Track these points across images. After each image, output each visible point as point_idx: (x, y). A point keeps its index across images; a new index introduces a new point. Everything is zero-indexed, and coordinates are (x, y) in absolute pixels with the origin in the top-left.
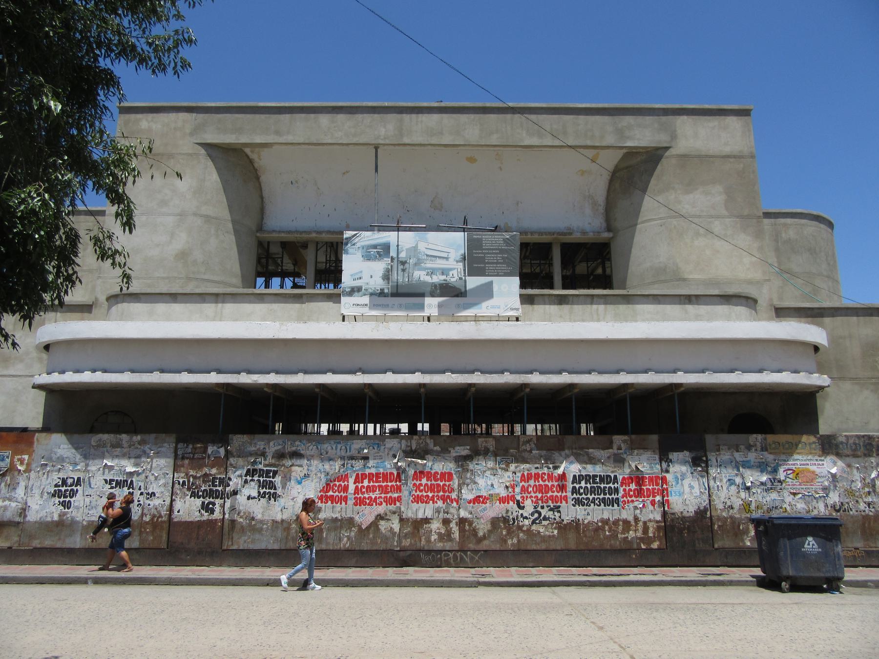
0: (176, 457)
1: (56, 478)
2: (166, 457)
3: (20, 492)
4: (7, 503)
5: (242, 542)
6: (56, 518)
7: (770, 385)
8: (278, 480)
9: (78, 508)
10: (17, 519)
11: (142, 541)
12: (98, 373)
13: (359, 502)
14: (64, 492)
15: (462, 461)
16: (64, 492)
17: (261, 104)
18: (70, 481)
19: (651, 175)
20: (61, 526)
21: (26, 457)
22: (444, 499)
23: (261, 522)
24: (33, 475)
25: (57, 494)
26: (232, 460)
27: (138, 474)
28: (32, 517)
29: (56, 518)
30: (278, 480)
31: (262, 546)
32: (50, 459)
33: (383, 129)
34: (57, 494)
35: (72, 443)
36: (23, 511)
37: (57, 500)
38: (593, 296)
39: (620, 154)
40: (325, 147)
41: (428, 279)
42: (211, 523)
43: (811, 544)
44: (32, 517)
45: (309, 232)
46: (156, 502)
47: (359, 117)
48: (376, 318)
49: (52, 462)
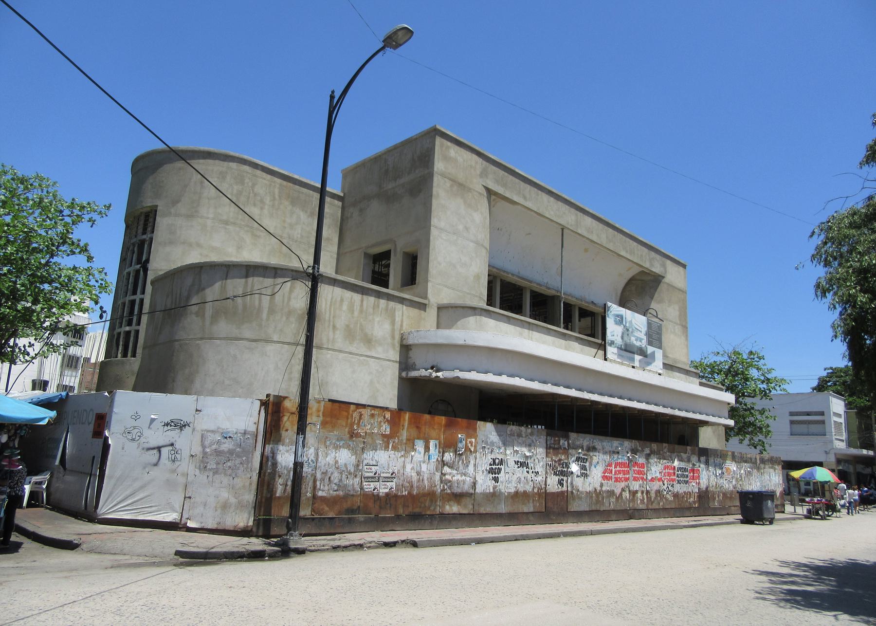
0: (547, 448)
1: (490, 457)
2: (540, 447)
3: (471, 468)
4: (464, 477)
5: (574, 506)
6: (492, 491)
7: (492, 384)
8: (587, 464)
9: (502, 482)
10: (472, 491)
11: (534, 506)
12: (504, 377)
13: (617, 480)
14: (494, 470)
15: (648, 457)
16: (494, 470)
17: (517, 170)
18: (497, 461)
19: (656, 290)
20: (494, 496)
21: (473, 440)
22: (642, 478)
23: (582, 492)
24: (478, 455)
25: (491, 471)
26: (570, 451)
27: (531, 457)
28: (479, 489)
29: (492, 491)
30: (587, 464)
31: (582, 509)
32: (486, 443)
33: (569, 217)
34: (491, 471)
35: (497, 431)
36: (474, 484)
37: (491, 476)
38: (379, 292)
39: (639, 269)
40: (542, 218)
41: (635, 342)
42: (562, 492)
43: (749, 504)
44: (479, 489)
45: (508, 273)
46: (539, 478)
47: (560, 203)
48: (619, 363)
49: (489, 446)
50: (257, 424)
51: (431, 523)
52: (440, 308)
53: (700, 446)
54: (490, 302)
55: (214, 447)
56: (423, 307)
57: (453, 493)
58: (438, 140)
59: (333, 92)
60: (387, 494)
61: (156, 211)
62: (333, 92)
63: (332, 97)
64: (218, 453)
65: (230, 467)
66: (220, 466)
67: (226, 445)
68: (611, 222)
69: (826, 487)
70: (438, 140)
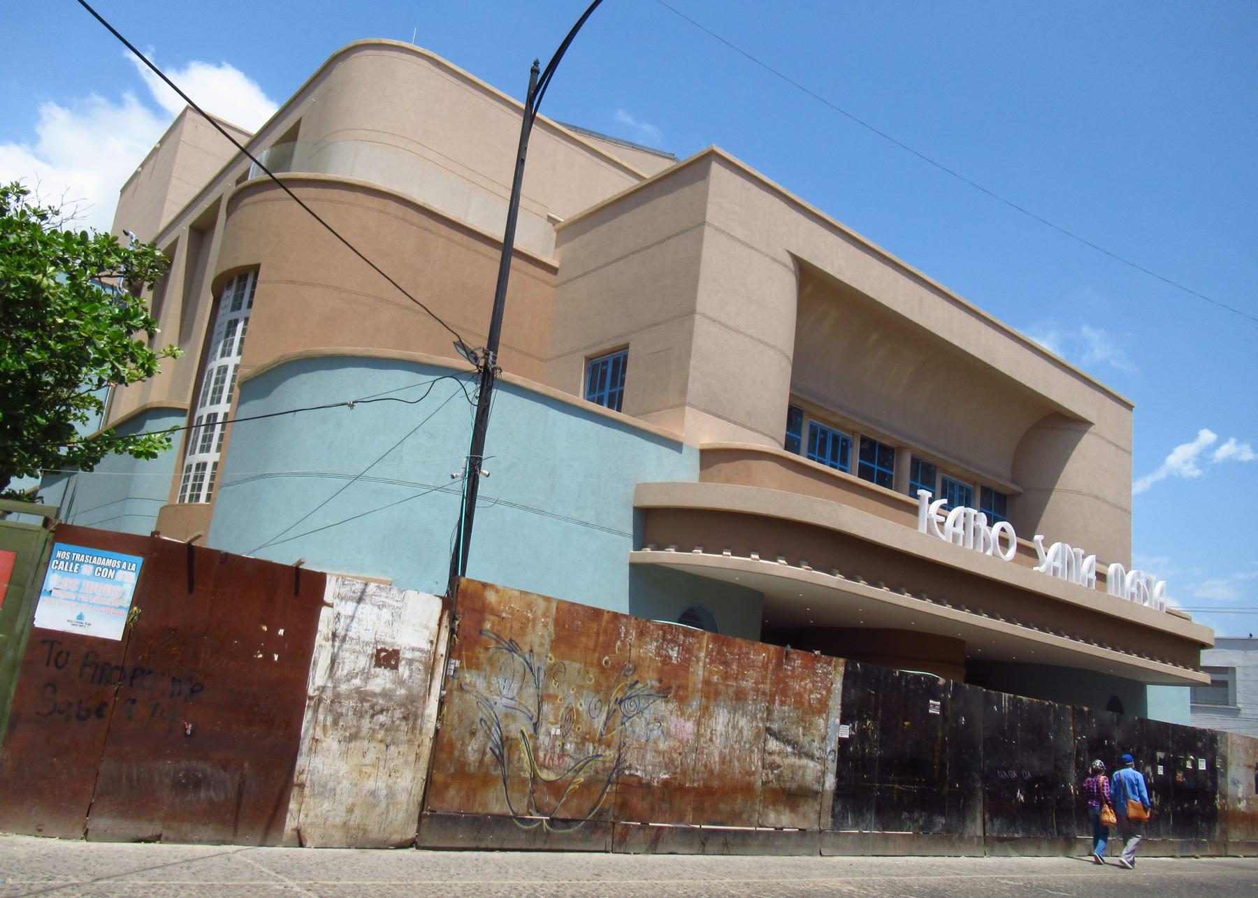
10: (816, 787)
50: (434, 643)
51: (30, 860)
52: (704, 452)
53: (38, 623)
54: (791, 445)
55: (357, 682)
56: (676, 445)
57: (784, 790)
58: (715, 167)
59: (536, 63)
60: (666, 784)
61: (626, 357)
62: (536, 63)
63: (534, 71)
64: (363, 696)
65: (382, 725)
66: (366, 723)
67: (378, 681)
68: (1116, 392)
69: (452, 800)
70: (715, 167)
